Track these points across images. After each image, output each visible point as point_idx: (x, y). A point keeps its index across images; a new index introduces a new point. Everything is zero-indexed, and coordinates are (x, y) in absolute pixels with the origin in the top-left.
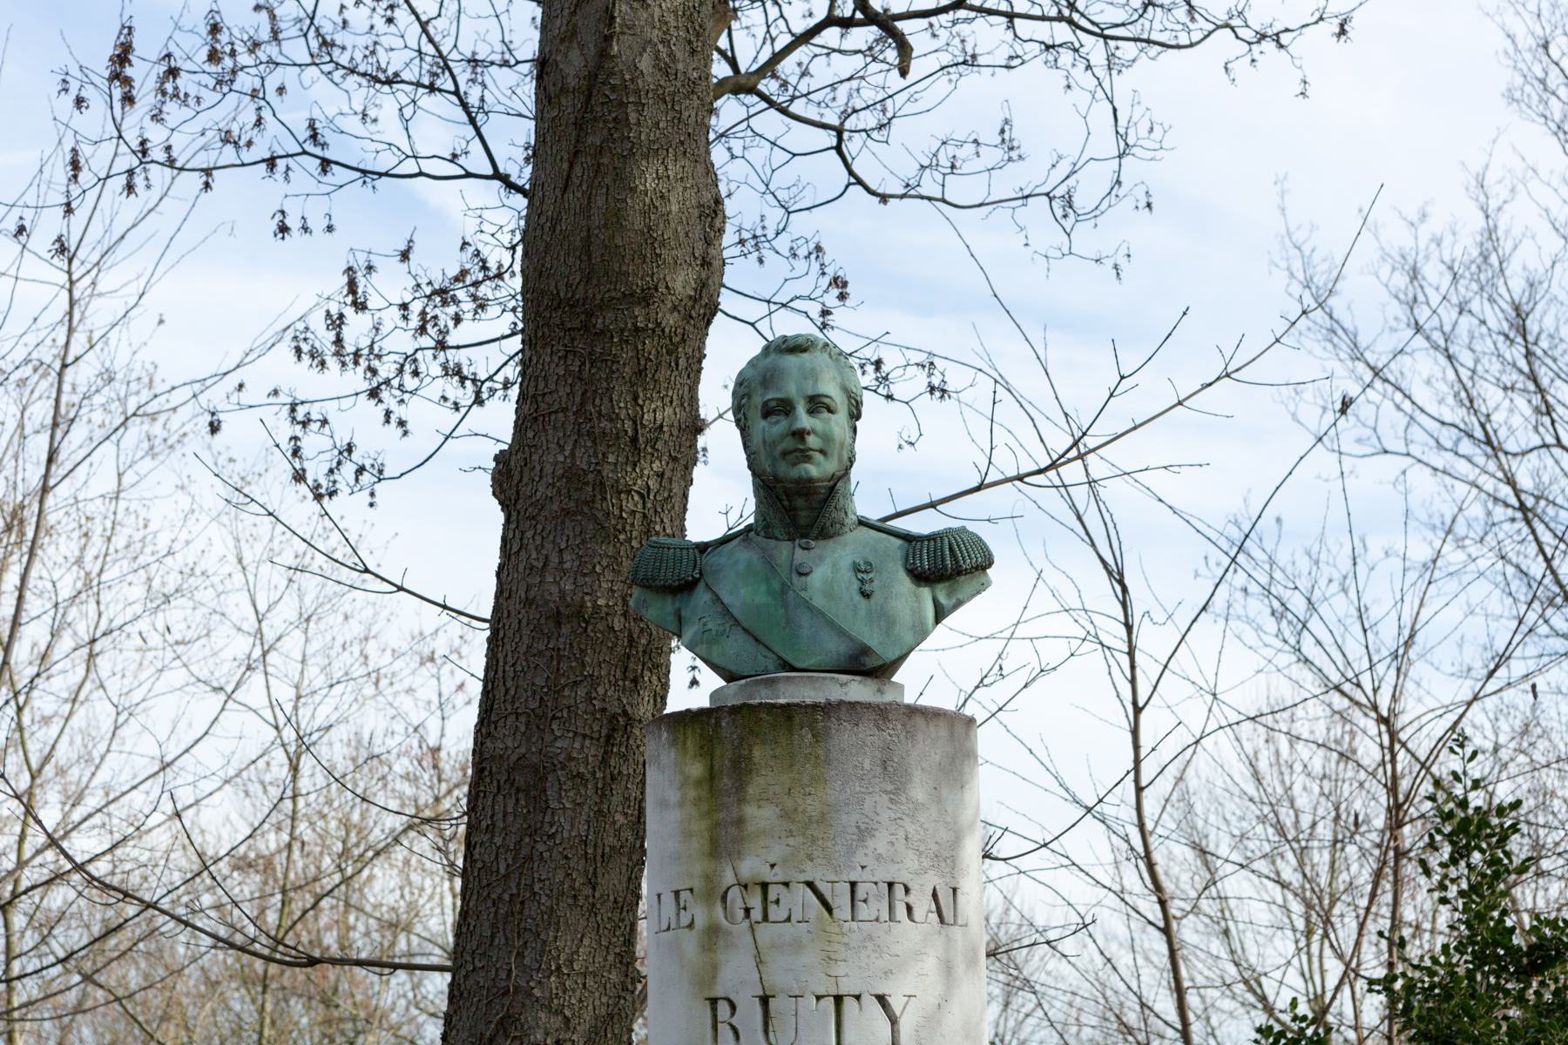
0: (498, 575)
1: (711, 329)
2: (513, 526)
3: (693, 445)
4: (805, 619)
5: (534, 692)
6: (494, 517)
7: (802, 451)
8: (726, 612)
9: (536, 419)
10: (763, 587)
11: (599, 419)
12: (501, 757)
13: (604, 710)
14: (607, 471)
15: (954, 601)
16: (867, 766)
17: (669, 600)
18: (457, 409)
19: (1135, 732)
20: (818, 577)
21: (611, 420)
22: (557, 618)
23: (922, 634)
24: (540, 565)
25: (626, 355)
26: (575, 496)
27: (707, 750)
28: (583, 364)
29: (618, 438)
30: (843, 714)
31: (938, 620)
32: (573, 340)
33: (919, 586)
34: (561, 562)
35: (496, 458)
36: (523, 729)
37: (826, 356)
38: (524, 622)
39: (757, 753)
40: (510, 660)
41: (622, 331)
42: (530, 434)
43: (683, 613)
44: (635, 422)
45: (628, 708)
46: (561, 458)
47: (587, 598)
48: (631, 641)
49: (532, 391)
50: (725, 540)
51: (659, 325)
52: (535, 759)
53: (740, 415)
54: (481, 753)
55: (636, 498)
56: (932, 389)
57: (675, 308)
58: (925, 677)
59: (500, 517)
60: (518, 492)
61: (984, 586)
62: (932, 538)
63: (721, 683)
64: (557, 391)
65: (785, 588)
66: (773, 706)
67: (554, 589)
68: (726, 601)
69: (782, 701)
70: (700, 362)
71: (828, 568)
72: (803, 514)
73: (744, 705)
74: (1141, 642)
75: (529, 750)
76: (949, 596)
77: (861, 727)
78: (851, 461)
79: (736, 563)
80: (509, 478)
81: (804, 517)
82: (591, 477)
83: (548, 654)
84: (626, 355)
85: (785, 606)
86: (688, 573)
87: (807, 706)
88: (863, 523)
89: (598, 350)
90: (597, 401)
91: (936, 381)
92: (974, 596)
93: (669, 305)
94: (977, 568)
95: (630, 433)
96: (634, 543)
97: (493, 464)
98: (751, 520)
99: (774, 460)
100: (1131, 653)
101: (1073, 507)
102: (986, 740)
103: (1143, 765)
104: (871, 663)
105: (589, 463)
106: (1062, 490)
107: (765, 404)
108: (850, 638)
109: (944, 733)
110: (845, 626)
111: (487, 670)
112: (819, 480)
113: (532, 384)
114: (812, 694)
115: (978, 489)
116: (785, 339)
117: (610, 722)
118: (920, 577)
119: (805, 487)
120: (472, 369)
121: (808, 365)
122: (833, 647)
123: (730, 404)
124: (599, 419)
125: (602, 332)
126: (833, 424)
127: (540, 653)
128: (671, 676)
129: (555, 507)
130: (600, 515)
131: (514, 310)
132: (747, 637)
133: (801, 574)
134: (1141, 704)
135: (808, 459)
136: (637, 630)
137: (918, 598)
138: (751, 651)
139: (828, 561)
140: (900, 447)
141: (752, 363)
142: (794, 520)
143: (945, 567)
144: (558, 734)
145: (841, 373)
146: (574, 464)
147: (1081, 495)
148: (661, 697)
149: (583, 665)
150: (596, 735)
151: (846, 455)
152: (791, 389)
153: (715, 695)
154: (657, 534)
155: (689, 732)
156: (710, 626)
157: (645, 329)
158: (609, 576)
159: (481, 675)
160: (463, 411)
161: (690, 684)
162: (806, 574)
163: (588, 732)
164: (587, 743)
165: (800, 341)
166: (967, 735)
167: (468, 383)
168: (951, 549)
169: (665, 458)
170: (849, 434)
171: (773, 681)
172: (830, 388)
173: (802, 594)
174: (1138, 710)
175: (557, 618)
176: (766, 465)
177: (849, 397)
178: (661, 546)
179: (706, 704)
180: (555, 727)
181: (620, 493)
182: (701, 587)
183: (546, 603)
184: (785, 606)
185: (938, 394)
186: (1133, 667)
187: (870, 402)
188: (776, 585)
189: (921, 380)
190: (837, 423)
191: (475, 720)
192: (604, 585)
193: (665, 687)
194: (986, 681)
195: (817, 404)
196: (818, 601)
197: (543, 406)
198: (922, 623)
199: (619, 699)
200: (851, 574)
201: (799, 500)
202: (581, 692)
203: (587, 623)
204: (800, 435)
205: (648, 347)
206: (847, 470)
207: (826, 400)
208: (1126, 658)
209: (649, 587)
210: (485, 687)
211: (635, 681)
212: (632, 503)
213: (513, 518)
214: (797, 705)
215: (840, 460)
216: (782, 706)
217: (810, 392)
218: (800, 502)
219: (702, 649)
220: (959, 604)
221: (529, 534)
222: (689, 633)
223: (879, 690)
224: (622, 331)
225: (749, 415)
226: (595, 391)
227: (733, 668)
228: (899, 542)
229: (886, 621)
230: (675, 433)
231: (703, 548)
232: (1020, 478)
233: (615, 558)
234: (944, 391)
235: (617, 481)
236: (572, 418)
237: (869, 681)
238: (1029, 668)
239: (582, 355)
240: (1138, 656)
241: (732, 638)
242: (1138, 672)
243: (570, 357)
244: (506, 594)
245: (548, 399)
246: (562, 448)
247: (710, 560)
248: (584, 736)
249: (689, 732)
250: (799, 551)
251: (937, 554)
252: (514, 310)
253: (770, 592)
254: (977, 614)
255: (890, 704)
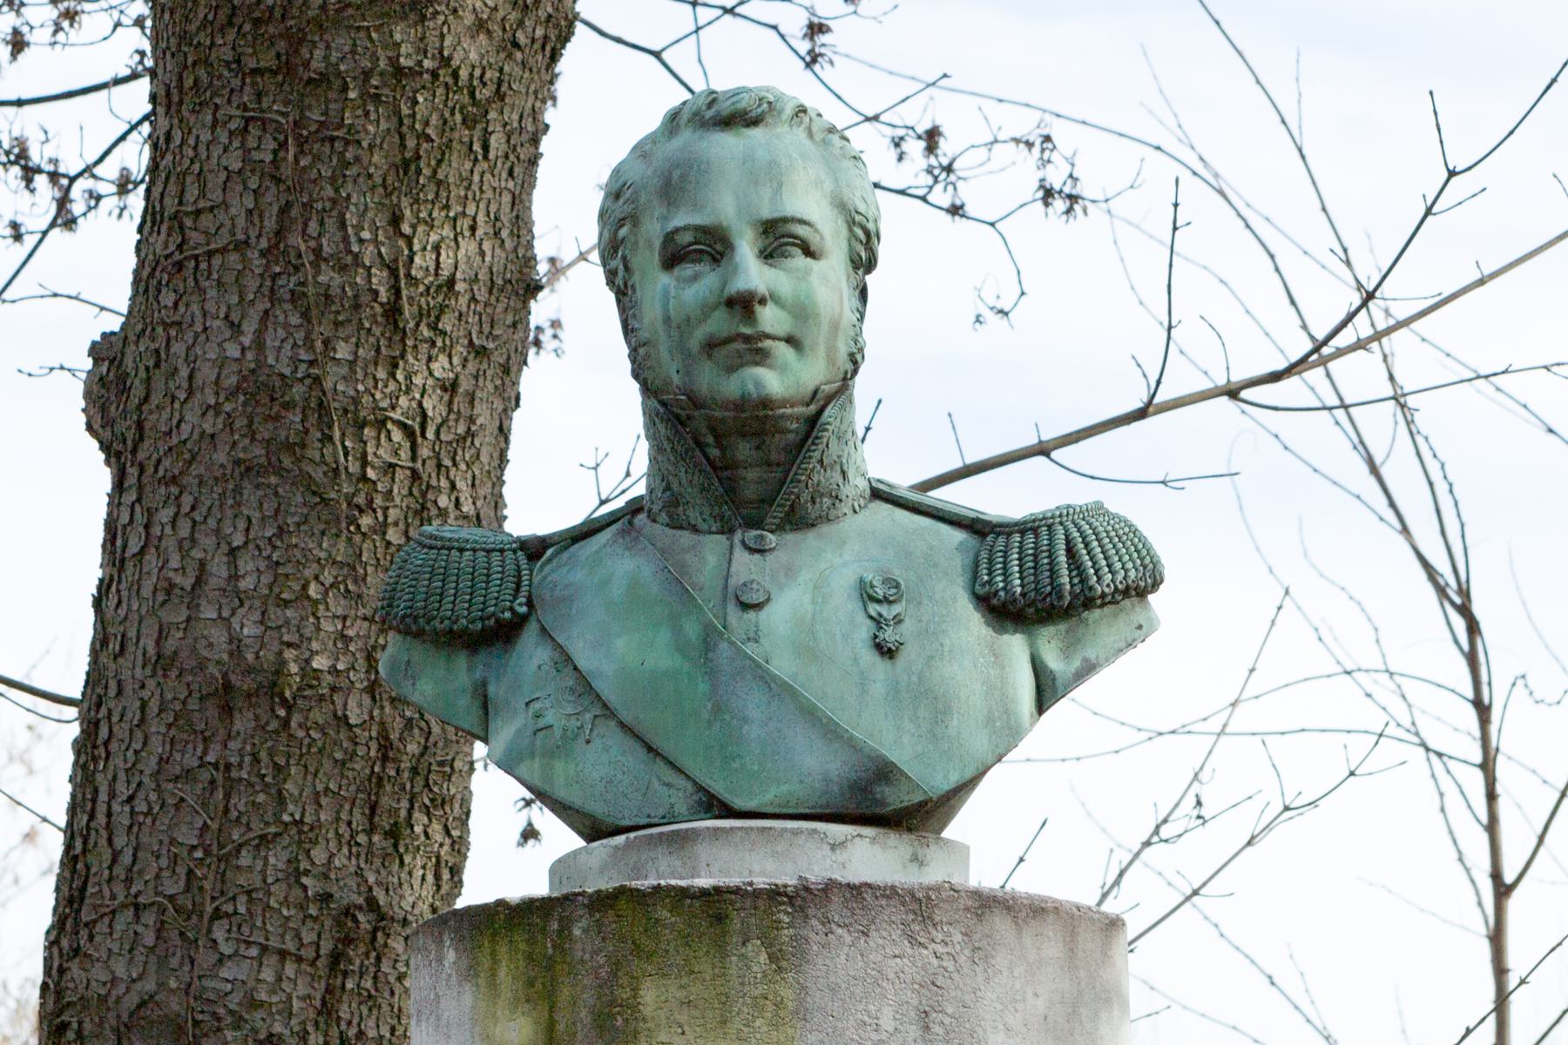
0: (98, 603)
1: (562, 66)
2: (130, 497)
3: (520, 321)
4: (752, 703)
5: (175, 859)
6: (89, 479)
7: (747, 339)
8: (584, 687)
9: (180, 266)
10: (664, 636)
11: (316, 266)
12: (103, 999)
13: (326, 898)
14: (333, 378)
15: (1077, 663)
16: (887, 1023)
17: (462, 661)
18: (18, 237)
19: (1497, 938)
20: (779, 616)
21: (343, 269)
22: (225, 698)
23: (1007, 737)
24: (188, 582)
25: (376, 127)
26: (264, 432)
27: (541, 986)
28: (283, 145)
29: (357, 307)
30: (836, 909)
31: (1042, 703)
32: (259, 96)
33: (1000, 629)
34: (234, 577)
35: (95, 351)
36: (149, 938)
37: (800, 134)
38: (154, 706)
39: (649, 996)
40: (123, 791)
41: (367, 74)
42: (168, 298)
43: (492, 690)
44: (394, 273)
45: (382, 899)
46: (233, 351)
47: (290, 654)
48: (386, 746)
49: (171, 204)
50: (586, 531)
51: (446, 61)
52: (175, 1005)
53: (616, 263)
54: (59, 994)
55: (397, 436)
56: (1048, 194)
57: (480, 26)
58: (989, 842)
59: (101, 478)
60: (140, 425)
61: (1142, 631)
62: (1028, 527)
63: (577, 842)
64: (225, 205)
65: (710, 638)
66: (684, 892)
67: (219, 636)
68: (581, 664)
69: (704, 882)
70: (535, 141)
71: (804, 593)
72: (752, 475)
73: (621, 891)
74: (1507, 735)
75: (161, 985)
76: (1067, 651)
77: (875, 939)
78: (855, 362)
79: (606, 583)
80: (124, 393)
81: (752, 480)
82: (298, 391)
83: (205, 775)
84: (376, 127)
85: (712, 673)
86: (502, 602)
87: (757, 894)
88: (879, 494)
89: (316, 115)
90: (313, 227)
91: (1056, 179)
92: (1120, 651)
93: (469, 19)
94: (1126, 593)
95: (384, 296)
96: (393, 535)
97: (88, 363)
98: (640, 489)
99: (688, 356)
100: (1487, 767)
101: (1361, 445)
102: (1144, 969)
103: (1516, 1003)
104: (896, 798)
105: (295, 361)
106: (1340, 413)
107: (669, 237)
108: (851, 744)
109: (1052, 948)
110: (843, 720)
111: (73, 810)
112: (784, 403)
113: (173, 188)
114: (770, 866)
115: (1141, 414)
116: (713, 98)
117: (339, 924)
118: (1005, 612)
119: (757, 416)
120: (50, 151)
121: (761, 154)
122: (815, 766)
123: (595, 240)
124: (316, 266)
125: (323, 79)
126: (814, 280)
127: (188, 775)
128: (473, 823)
129: (221, 457)
130: (318, 474)
131: (139, 23)
132: (630, 742)
133: (745, 607)
134: (1509, 878)
135: (762, 357)
136: (398, 724)
137: (998, 656)
138: (653, 767)
139: (805, 577)
140: (978, 320)
141: (642, 151)
142: (731, 490)
143: (1057, 590)
144: (226, 949)
145: (834, 173)
146: (260, 363)
147: (1378, 424)
148: (451, 872)
149: (281, 800)
150: (308, 953)
151: (843, 349)
152: (725, 206)
153: (559, 869)
154: (443, 513)
155: (503, 950)
156: (549, 718)
157: (416, 72)
158: (337, 605)
159: (62, 820)
160: (30, 241)
161: (509, 847)
162: (758, 607)
163: (290, 945)
164: (290, 969)
165: (745, 102)
166: (1105, 954)
167: (41, 181)
168: (1071, 552)
169: (460, 349)
170: (850, 301)
171: (681, 840)
172: (808, 203)
173: (749, 649)
174: (1503, 890)
175: (225, 698)
176: (670, 369)
177: (851, 223)
178: (447, 546)
179: (540, 888)
180: (219, 934)
181: (361, 425)
182: (530, 633)
183: (202, 666)
184: (712, 673)
185: (1059, 205)
186: (1491, 796)
187: (901, 228)
188: (692, 629)
189: (1024, 173)
190: (826, 279)
191: (47, 920)
192: (327, 626)
193: (460, 846)
194: (1165, 832)
195: (780, 238)
196: (782, 665)
197: (195, 237)
198: (1007, 710)
199: (359, 873)
200: (854, 606)
201: (741, 454)
202: (277, 859)
203: (289, 708)
204: (744, 304)
205: (421, 110)
206: (847, 379)
207: (801, 230)
208: (1478, 777)
209: (419, 634)
210: (69, 847)
211: (393, 834)
212: (388, 448)
213: (131, 480)
214: (737, 891)
215: (831, 359)
216: (704, 893)
217: (767, 213)
218: (743, 450)
219: (532, 768)
220: (1088, 669)
221: (165, 515)
222: (506, 731)
223: (915, 858)
224: (367, 74)
225: (635, 263)
226: (308, 206)
227: (598, 809)
228: (958, 536)
229: (931, 705)
230: (482, 295)
231: (535, 549)
232: (1233, 393)
233: (351, 566)
234: (1073, 198)
235: (356, 401)
236: (258, 263)
237: (892, 838)
238: (1258, 803)
239: (279, 129)
240: (1502, 768)
241: (597, 743)
242: (1503, 805)
243: (254, 131)
244: (114, 646)
245: (206, 221)
246: (236, 328)
247: (552, 575)
248: (283, 954)
249: (503, 950)
250: (741, 557)
251: (1041, 563)
252: (139, 23)
253: (680, 647)
254: (1132, 686)
255: (937, 888)
